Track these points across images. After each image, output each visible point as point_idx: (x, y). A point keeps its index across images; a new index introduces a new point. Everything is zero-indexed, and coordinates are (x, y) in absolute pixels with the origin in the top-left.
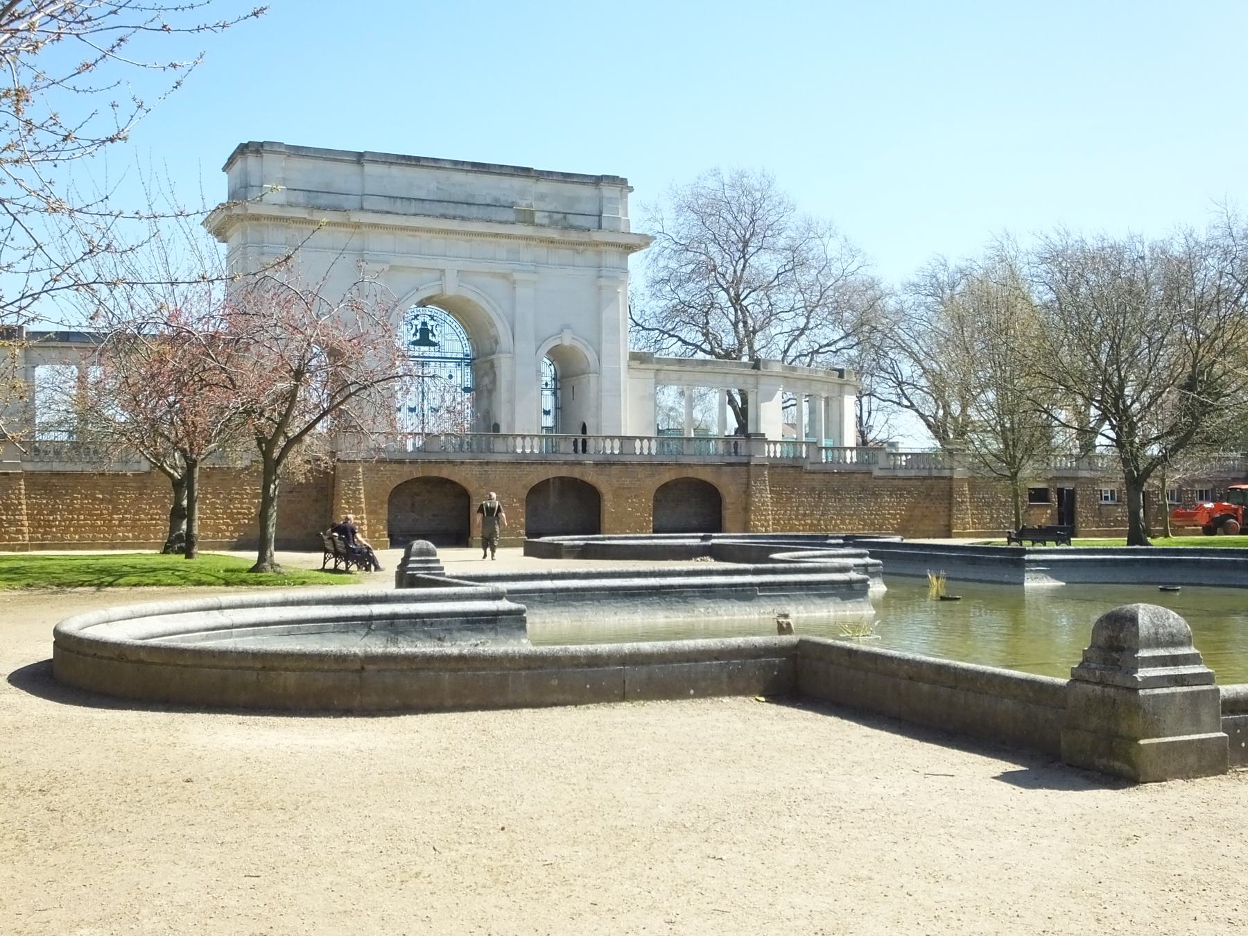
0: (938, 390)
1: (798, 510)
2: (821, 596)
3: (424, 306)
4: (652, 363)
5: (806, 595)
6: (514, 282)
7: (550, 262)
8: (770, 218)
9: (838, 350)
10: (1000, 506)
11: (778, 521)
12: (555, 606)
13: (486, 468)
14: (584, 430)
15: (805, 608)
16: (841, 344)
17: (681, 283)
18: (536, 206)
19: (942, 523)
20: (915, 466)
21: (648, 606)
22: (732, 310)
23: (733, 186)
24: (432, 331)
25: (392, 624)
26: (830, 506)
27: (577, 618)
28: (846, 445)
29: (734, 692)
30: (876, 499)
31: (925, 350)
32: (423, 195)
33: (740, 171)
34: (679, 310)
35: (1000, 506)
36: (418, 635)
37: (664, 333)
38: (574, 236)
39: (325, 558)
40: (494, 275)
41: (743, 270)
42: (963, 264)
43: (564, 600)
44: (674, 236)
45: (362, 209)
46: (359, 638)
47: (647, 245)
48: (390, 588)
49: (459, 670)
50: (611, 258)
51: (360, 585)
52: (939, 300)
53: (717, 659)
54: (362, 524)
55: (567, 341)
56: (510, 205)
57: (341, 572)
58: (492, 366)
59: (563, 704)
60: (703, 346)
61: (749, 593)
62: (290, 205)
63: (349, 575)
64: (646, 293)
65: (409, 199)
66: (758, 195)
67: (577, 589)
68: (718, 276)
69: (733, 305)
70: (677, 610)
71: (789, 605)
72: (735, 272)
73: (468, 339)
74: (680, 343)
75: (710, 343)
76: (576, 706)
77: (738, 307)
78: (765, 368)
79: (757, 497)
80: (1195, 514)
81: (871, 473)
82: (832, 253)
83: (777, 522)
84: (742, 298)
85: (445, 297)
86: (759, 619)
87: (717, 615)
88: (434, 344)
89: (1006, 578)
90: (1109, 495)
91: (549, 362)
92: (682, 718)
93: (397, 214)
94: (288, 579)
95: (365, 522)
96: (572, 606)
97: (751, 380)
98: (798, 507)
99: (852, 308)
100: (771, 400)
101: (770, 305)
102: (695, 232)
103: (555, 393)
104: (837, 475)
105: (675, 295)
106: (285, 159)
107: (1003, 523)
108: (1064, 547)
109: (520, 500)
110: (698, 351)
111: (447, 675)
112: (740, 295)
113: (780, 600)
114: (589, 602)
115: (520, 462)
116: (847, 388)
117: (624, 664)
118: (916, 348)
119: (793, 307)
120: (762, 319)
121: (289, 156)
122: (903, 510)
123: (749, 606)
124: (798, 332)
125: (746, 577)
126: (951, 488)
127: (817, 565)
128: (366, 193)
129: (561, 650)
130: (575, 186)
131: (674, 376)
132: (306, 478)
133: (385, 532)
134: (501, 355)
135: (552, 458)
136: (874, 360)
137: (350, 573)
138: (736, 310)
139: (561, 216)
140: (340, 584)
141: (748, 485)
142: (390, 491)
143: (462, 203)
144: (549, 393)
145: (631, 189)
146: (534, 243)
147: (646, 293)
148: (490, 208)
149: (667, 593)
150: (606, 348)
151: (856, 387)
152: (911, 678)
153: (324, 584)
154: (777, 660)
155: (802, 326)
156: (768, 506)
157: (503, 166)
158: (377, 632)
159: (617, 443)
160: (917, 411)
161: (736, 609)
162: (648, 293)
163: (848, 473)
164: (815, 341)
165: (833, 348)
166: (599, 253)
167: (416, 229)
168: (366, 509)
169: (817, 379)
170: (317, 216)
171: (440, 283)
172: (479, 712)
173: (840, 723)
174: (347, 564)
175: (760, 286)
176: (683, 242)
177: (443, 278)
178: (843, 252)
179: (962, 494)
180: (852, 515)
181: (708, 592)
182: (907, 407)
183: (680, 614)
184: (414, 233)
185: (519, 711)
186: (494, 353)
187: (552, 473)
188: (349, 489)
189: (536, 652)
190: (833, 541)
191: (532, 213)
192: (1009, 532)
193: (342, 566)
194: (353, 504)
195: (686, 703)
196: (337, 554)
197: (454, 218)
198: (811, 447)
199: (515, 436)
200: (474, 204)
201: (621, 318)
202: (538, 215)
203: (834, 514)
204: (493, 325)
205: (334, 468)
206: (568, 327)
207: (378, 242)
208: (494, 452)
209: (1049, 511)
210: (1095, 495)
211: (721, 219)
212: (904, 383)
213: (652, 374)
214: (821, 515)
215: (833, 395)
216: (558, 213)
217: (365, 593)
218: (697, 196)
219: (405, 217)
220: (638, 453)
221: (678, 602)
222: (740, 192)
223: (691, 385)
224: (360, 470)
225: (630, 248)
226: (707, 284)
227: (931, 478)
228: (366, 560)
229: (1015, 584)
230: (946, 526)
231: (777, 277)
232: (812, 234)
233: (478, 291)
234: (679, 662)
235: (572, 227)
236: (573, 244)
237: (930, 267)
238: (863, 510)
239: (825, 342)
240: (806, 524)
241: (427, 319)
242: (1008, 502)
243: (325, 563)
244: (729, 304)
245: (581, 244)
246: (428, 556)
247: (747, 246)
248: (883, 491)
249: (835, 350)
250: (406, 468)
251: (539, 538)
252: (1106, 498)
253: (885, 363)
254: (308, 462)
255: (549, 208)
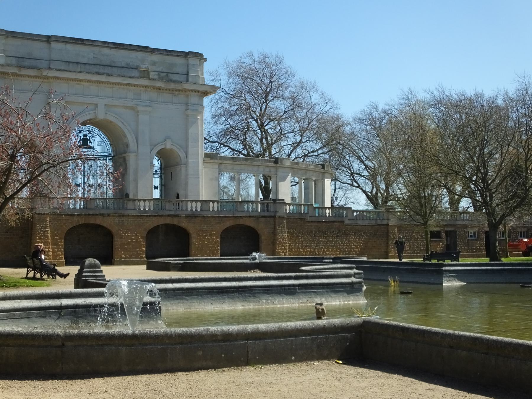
0: (373, 177)
1: (302, 243)
2: (336, 292)
3: (85, 126)
4: (217, 159)
5: (326, 291)
6: (138, 112)
7: (158, 101)
8: (280, 81)
9: (318, 155)
10: (415, 241)
11: (292, 249)
12: (174, 299)
13: (123, 219)
14: (178, 197)
15: (326, 300)
16: (320, 152)
17: (231, 116)
18: (151, 68)
19: (383, 250)
20: (362, 218)
21: (231, 299)
22: (259, 132)
23: (260, 62)
24: (89, 140)
25: (75, 312)
26: (321, 241)
27: (188, 307)
28: (326, 206)
29: (321, 357)
30: (347, 237)
31: (366, 155)
32: (85, 60)
33: (264, 54)
34: (229, 132)
35: (415, 241)
36: (91, 319)
37: (221, 144)
38: (172, 86)
39: (28, 271)
40: (126, 107)
41: (266, 109)
42: (387, 108)
43: (180, 296)
44: (227, 89)
45: (49, 68)
46: (53, 321)
47: (214, 92)
48: (70, 288)
49: (133, 345)
50: (194, 99)
51: (50, 287)
52: (373, 127)
53: (310, 335)
54: (49, 251)
55: (168, 146)
56: (136, 68)
57: (38, 279)
58: (125, 160)
59: (206, 368)
60: (243, 152)
61: (292, 290)
62: (8, 65)
63: (43, 281)
64: (211, 121)
65: (77, 63)
66: (274, 68)
67: (188, 289)
68: (252, 112)
69: (260, 129)
70: (250, 302)
71: (316, 297)
72: (261, 110)
73: (110, 145)
74: (230, 150)
75: (247, 150)
76: (215, 370)
77: (263, 130)
78: (281, 162)
79: (280, 236)
80: (518, 245)
81: (344, 222)
82: (315, 101)
83: (291, 250)
84: (265, 125)
85: (97, 120)
86: (299, 306)
87: (273, 304)
88: (90, 147)
89: (432, 280)
90: (473, 234)
91: (157, 158)
92: (293, 378)
93: (70, 71)
94: (5, 283)
95: (51, 250)
96: (185, 299)
97: (273, 170)
98: (302, 241)
99: (326, 131)
100: (285, 181)
101: (281, 129)
102: (239, 87)
103: (160, 177)
104: (325, 223)
105: (227, 123)
106: (5, 38)
107: (416, 250)
108: (455, 263)
109: (142, 238)
110: (240, 154)
111: (124, 349)
112: (264, 123)
113: (311, 295)
114: (196, 297)
115: (142, 215)
116: (326, 175)
117: (247, 340)
118: (361, 154)
119: (293, 130)
120: (276, 137)
121: (7, 37)
122: (362, 243)
123: (292, 299)
124: (296, 145)
125: (291, 281)
126: (388, 231)
127: (332, 273)
128: (52, 59)
129: (204, 330)
130: (173, 57)
131: (229, 167)
132: (16, 223)
133: (63, 256)
134: (130, 154)
135: (161, 213)
136: (338, 160)
137: (44, 280)
138: (261, 132)
139: (165, 74)
140: (38, 286)
141: (275, 229)
142: (66, 232)
143: (108, 66)
144: (157, 176)
145: (205, 60)
146: (149, 89)
147: (211, 121)
148: (124, 69)
149: (243, 291)
150: (191, 150)
151: (331, 174)
152: (451, 347)
153: (27, 286)
154: (349, 335)
155: (298, 141)
156: (286, 241)
157: (132, 45)
158: (65, 317)
159: (199, 205)
160: (362, 189)
161: (285, 300)
162: (212, 122)
163: (330, 223)
164: (306, 149)
165: (316, 154)
166: (187, 96)
167: (81, 80)
168: (51, 242)
169: (311, 169)
170: (24, 72)
171: (94, 111)
172: (148, 375)
173: (404, 379)
174: (41, 275)
175: (275, 118)
176: (232, 93)
177: (96, 108)
178: (321, 100)
179: (394, 234)
180: (334, 246)
181: (268, 290)
182: (356, 187)
183: (251, 304)
184: (80, 83)
185: (176, 374)
186: (126, 153)
187: (161, 221)
188: (41, 231)
189: (187, 331)
190: (326, 261)
191: (148, 73)
192: (424, 255)
193: (38, 275)
194: (44, 239)
195: (290, 366)
196: (35, 269)
197: (103, 74)
198: (310, 207)
199: (139, 200)
200: (115, 67)
201: (199, 133)
202: (152, 73)
203: (323, 245)
204: (125, 136)
205: (32, 218)
206: (169, 138)
207: (61, 88)
208: (127, 209)
209: (441, 244)
210: (465, 234)
211: (253, 80)
212: (355, 173)
213: (217, 166)
214: (316, 246)
215: (318, 179)
216: (163, 72)
217: (57, 291)
218: (240, 67)
219: (75, 73)
220: (211, 210)
221: (250, 296)
222: (264, 66)
223: (239, 173)
224: (48, 219)
225: (205, 94)
226: (245, 117)
227: (377, 225)
228: (52, 272)
229: (437, 284)
230: (385, 252)
231: (284, 113)
232: (304, 90)
233: (116, 116)
234: (285, 337)
235: (171, 81)
236: (172, 91)
237: (368, 110)
238: (339, 243)
239: (312, 150)
240: (307, 251)
241: (87, 133)
242: (419, 238)
243: (27, 274)
244: (258, 128)
245: (177, 90)
246: (95, 268)
247: (268, 96)
248: (351, 232)
249: (316, 154)
250: (75, 219)
251: (155, 259)
252: (471, 236)
253: (344, 162)
254: (18, 214)
255: (158, 69)
